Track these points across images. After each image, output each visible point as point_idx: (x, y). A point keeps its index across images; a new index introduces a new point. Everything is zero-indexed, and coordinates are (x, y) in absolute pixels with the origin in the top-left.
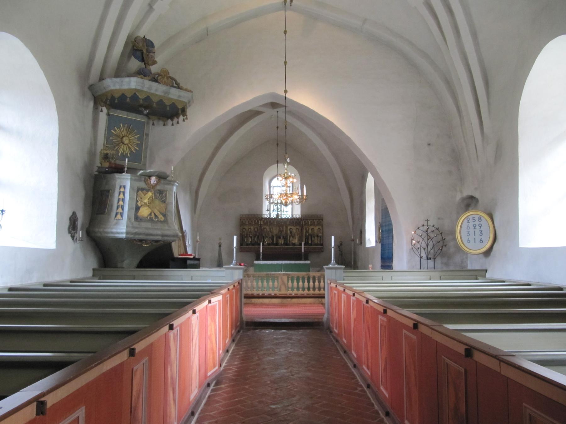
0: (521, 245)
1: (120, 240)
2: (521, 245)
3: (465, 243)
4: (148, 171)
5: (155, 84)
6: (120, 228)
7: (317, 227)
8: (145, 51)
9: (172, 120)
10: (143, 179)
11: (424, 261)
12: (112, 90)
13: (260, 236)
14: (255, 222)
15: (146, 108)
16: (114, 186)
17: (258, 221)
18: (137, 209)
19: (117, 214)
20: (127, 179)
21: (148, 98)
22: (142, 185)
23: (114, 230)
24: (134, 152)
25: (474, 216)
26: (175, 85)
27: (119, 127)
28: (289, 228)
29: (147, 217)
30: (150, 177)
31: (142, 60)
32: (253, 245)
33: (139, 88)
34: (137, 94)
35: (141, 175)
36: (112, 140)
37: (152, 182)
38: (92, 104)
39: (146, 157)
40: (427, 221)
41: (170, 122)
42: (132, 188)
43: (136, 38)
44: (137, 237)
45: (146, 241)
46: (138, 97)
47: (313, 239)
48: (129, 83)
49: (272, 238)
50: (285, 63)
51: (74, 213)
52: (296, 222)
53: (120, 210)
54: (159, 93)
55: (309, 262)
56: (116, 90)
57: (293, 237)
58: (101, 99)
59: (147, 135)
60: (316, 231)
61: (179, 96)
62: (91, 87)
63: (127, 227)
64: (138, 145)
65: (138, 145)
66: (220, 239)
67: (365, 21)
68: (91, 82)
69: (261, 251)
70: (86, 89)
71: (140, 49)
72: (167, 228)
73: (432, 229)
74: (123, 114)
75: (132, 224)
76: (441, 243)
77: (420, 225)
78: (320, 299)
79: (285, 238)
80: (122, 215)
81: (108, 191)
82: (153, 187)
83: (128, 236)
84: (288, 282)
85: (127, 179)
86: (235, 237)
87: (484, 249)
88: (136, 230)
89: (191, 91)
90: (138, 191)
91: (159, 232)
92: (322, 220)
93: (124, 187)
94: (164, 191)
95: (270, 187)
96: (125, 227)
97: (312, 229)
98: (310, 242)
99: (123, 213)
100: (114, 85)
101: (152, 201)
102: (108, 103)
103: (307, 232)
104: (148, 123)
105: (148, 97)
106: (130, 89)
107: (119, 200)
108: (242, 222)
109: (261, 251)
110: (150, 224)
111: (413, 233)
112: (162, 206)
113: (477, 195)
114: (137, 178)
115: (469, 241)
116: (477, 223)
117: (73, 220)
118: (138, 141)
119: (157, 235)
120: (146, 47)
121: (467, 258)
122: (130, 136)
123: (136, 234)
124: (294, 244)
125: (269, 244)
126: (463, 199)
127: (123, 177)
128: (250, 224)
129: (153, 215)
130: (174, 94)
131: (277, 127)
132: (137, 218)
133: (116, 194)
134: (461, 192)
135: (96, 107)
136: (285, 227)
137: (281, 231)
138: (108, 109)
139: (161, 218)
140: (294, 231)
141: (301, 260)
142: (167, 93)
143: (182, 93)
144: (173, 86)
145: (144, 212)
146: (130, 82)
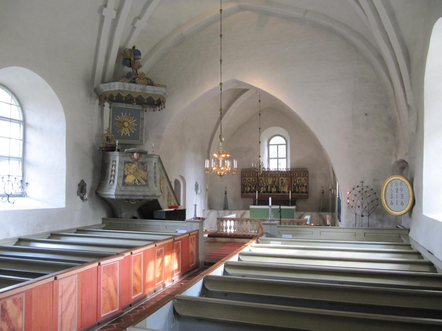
0: (64, 206)
2: (64, 206)
3: (389, 203)
5: (133, 85)
6: (112, 192)
7: (304, 178)
8: (132, 59)
14: (253, 174)
17: (255, 174)
18: (125, 177)
23: (108, 193)
24: (133, 132)
27: (120, 115)
28: (280, 179)
30: (133, 153)
33: (122, 89)
35: (126, 152)
36: (116, 125)
37: (135, 157)
38: (97, 102)
42: (120, 162)
45: (132, 200)
49: (267, 187)
50: (221, 61)
51: (82, 182)
52: (286, 174)
53: (112, 178)
54: (138, 91)
55: (294, 207)
56: (107, 91)
57: (283, 186)
58: (103, 98)
59: (143, 119)
61: (154, 91)
62: (95, 90)
63: (116, 190)
64: (136, 127)
65: (136, 127)
66: (226, 188)
68: (95, 86)
70: (93, 91)
72: (147, 190)
74: (123, 105)
75: (120, 188)
79: (277, 187)
80: (113, 181)
81: (107, 164)
82: (137, 160)
88: (123, 193)
89: (165, 86)
90: (125, 164)
91: (141, 194)
92: (308, 172)
95: (269, 145)
98: (297, 191)
100: (106, 88)
102: (114, 99)
104: (143, 110)
108: (243, 175)
111: (348, 193)
114: (124, 155)
115: (392, 203)
116: (399, 187)
120: (133, 56)
122: (129, 121)
123: (122, 195)
125: (264, 192)
128: (249, 176)
129: (137, 181)
131: (260, 101)
132: (124, 184)
133: (111, 167)
134: (396, 156)
135: (101, 105)
137: (274, 182)
138: (110, 104)
139: (143, 182)
140: (284, 181)
141: (288, 205)
142: (144, 89)
143: (156, 89)
145: (130, 179)
146: (115, 85)
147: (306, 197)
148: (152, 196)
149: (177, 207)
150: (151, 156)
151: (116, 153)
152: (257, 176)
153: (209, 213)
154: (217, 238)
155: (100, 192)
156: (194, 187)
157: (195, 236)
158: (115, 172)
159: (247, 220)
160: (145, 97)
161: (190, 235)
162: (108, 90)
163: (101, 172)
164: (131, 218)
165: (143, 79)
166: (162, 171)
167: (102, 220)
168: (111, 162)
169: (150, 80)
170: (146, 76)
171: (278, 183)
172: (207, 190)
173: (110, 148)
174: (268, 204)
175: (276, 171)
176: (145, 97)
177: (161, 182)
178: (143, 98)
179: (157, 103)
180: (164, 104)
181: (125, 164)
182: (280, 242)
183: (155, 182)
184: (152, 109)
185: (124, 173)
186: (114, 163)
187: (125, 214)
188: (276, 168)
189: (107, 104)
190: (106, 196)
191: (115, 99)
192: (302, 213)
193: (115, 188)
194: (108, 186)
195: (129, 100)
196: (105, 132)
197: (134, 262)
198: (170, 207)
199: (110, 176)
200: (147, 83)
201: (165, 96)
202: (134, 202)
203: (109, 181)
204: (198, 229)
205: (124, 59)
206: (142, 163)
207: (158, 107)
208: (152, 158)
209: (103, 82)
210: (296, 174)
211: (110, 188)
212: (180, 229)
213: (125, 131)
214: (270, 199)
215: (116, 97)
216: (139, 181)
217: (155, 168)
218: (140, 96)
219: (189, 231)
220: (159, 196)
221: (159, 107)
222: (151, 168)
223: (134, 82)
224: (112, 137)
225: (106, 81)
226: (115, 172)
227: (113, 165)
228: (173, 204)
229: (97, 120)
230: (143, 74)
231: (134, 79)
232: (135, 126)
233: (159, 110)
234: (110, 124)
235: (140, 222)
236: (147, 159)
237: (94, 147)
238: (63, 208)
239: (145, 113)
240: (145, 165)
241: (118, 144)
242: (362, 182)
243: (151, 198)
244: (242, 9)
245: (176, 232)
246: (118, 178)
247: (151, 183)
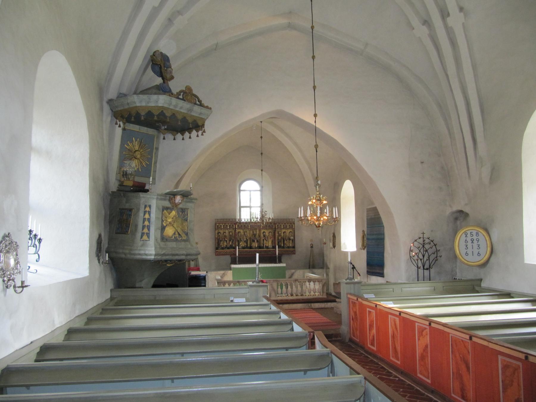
0: (526, 261)
2: (526, 261)
6: (150, 250)
7: (289, 230)
8: (162, 66)
9: (183, 135)
10: (168, 198)
11: (421, 271)
12: (136, 107)
13: (235, 239)
14: (230, 226)
15: (164, 123)
17: (233, 226)
18: (163, 228)
19: (143, 234)
21: (162, 114)
22: (167, 204)
24: (145, 166)
25: (471, 231)
26: (197, 102)
28: (262, 231)
29: (172, 237)
31: (161, 75)
32: (228, 248)
33: (166, 106)
40: (423, 233)
41: (179, 136)
42: (157, 207)
43: (155, 52)
44: (165, 258)
47: (285, 242)
48: (157, 102)
50: (314, 87)
53: (146, 230)
55: (283, 265)
56: (141, 106)
59: (157, 149)
60: (287, 234)
63: (156, 248)
67: (366, 45)
69: (237, 255)
71: (159, 63)
73: (427, 241)
75: (159, 245)
76: (436, 254)
77: (417, 238)
78: (310, 304)
80: (148, 235)
81: (131, 210)
83: (156, 257)
84: (278, 288)
87: (482, 262)
90: (163, 211)
91: (184, 252)
92: (294, 224)
93: (150, 206)
96: (153, 248)
97: (284, 233)
99: (149, 233)
100: (141, 102)
101: (175, 220)
102: (133, 119)
103: (279, 235)
104: (158, 137)
105: (174, 114)
106: (157, 106)
107: (144, 220)
109: (237, 255)
110: (175, 243)
113: (466, 210)
114: (163, 197)
115: (467, 254)
116: (475, 237)
117: (99, 242)
119: (183, 255)
121: (456, 267)
122: (141, 151)
123: (164, 255)
124: (267, 247)
125: (243, 248)
126: (453, 213)
129: (177, 235)
130: (197, 111)
132: (164, 239)
133: (141, 214)
136: (258, 231)
138: (124, 123)
139: (184, 237)
140: (267, 234)
141: (276, 263)
142: (190, 110)
143: (197, 109)
144: (195, 104)
145: (169, 231)
147: (294, 253)
152: (235, 228)
154: (312, 304)
158: (149, 222)
159: (229, 283)
162: (144, 104)
171: (259, 236)
174: (254, 262)
175: (249, 223)
181: (163, 211)
182: (391, 302)
185: (162, 224)
188: (249, 218)
192: (293, 271)
194: (138, 242)
197: (374, 339)
210: (281, 226)
214: (257, 255)
216: (179, 234)
226: (149, 222)
238: (87, 277)
242: (423, 233)
244: (290, 26)
245: (232, 301)
246: (156, 230)
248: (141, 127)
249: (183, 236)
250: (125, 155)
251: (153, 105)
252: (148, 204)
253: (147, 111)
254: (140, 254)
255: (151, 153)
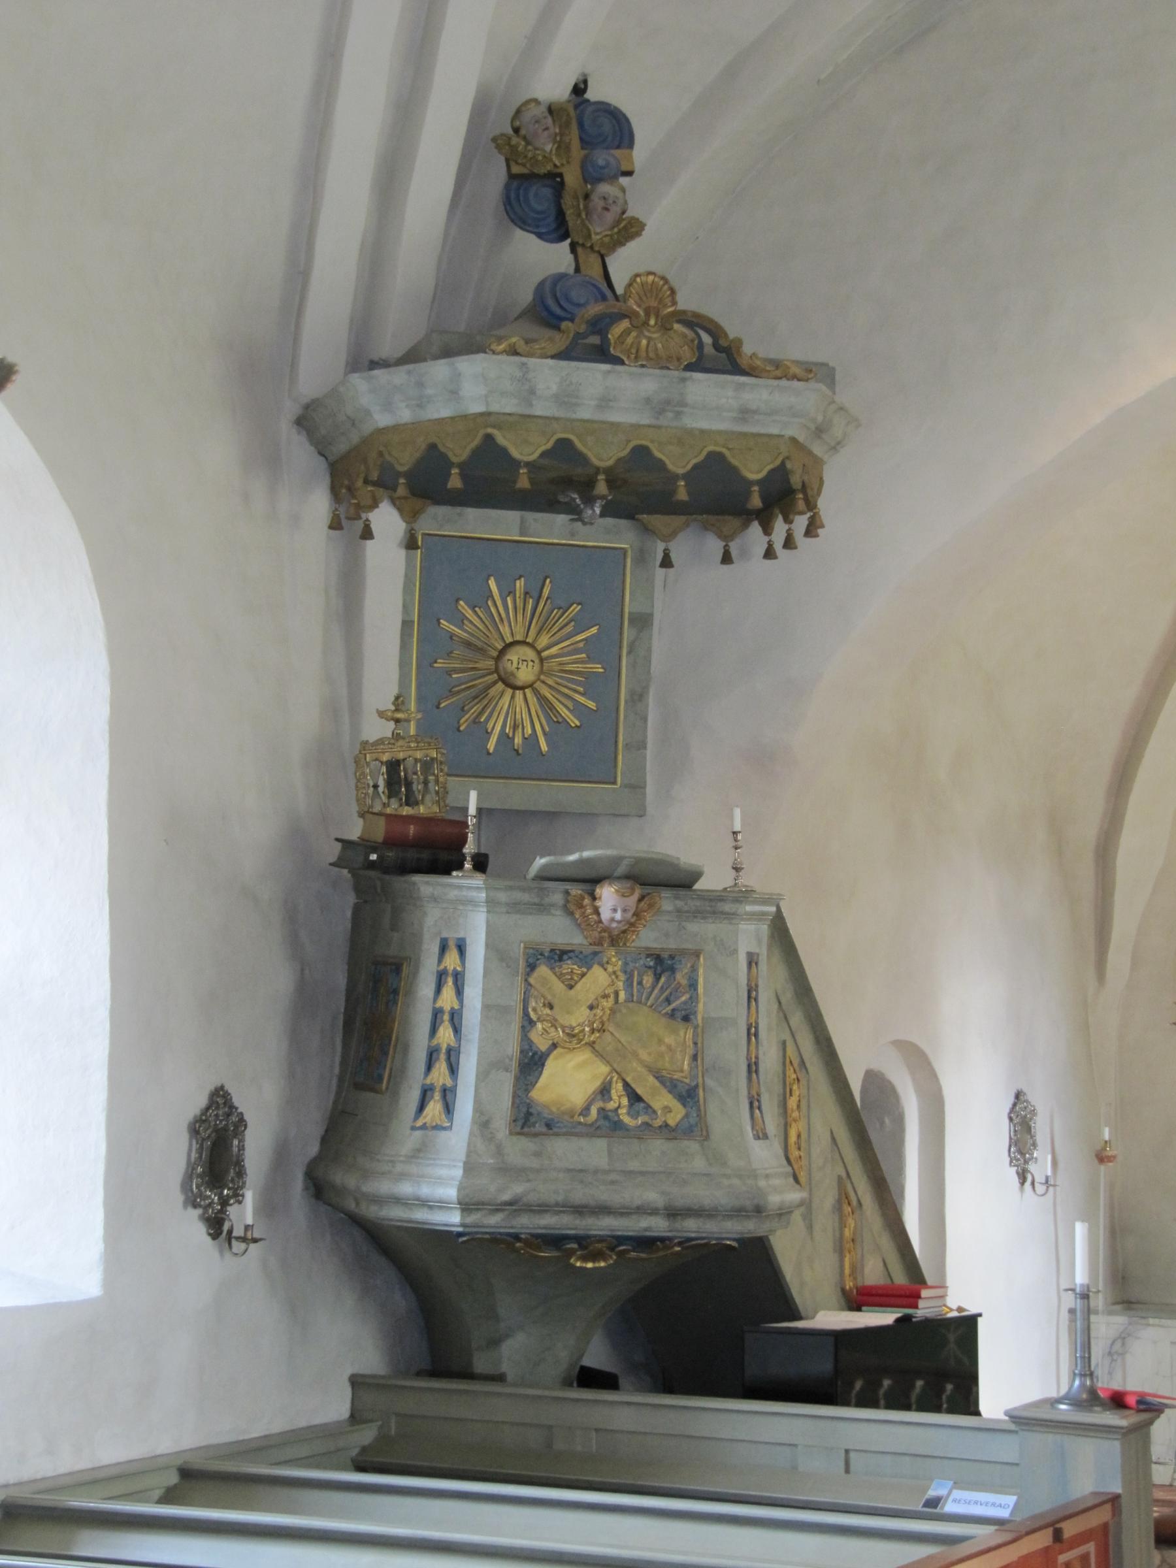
1: (440, 1238)
4: (572, 858)
5: (592, 377)
6: (437, 1177)
8: (572, 178)
10: (558, 898)
12: (381, 431)
16: (417, 939)
18: (531, 1063)
19: (426, 1094)
20: (472, 902)
23: (406, 1189)
29: (586, 1110)
33: (508, 406)
34: (501, 439)
35: (544, 877)
36: (454, 673)
37: (606, 915)
38: (319, 504)
39: (643, 745)
44: (526, 1224)
45: (586, 1244)
46: (504, 452)
51: (220, 1099)
56: (396, 428)
58: (358, 474)
59: (643, 621)
61: (745, 413)
62: (307, 421)
65: (590, 684)
68: (309, 385)
70: (285, 428)
75: (499, 1151)
81: (397, 968)
82: (616, 939)
83: (472, 1218)
85: (472, 902)
86: (1080, 1229)
88: (517, 1189)
91: (652, 1196)
93: (461, 949)
94: (683, 952)
96: (458, 1173)
100: (389, 405)
102: (455, 482)
104: (641, 558)
106: (465, 417)
110: (601, 1144)
112: (669, 1040)
114: (526, 897)
118: (590, 659)
120: (577, 152)
122: (543, 641)
123: (515, 1206)
127: (453, 894)
129: (618, 1098)
132: (528, 1119)
133: (425, 989)
135: (348, 520)
138: (411, 516)
139: (673, 1111)
143: (758, 393)
145: (569, 1081)
146: (456, 376)
148: (739, 1212)
149: (911, 1298)
150: (717, 906)
151: (466, 884)
153: (1123, 1338)
155: (341, 1177)
156: (1004, 1130)
157: (1091, 1547)
160: (678, 462)
161: (1058, 1535)
162: (405, 415)
163: (361, 1024)
164: (567, 1383)
165: (665, 327)
166: (797, 1019)
167: (348, 1392)
168: (431, 948)
169: (715, 331)
170: (681, 306)
172: (1102, 1158)
173: (418, 844)
176: (678, 462)
177: (792, 1102)
178: (661, 466)
179: (760, 499)
180: (811, 505)
181: (532, 967)
183: (754, 1103)
184: (715, 546)
186: (451, 961)
187: (527, 1345)
189: (387, 520)
190: (395, 1213)
191: (446, 477)
193: (461, 1154)
194: (403, 1136)
195: (562, 481)
196: (377, 729)
198: (857, 1300)
199: (419, 1056)
200: (688, 356)
201: (818, 449)
202: (594, 1257)
203: (412, 1096)
204: (1119, 1490)
205: (512, 176)
206: (658, 959)
207: (755, 528)
208: (730, 916)
209: (363, 361)
211: (419, 1152)
212: (957, 1485)
213: (512, 717)
215: (465, 468)
216: (635, 1098)
217: (752, 995)
218: (641, 453)
219: (1045, 1501)
220: (783, 1214)
221: (767, 529)
222: (719, 993)
223: (602, 354)
224: (427, 765)
225: (388, 347)
226: (457, 1030)
227: (441, 977)
228: (873, 1275)
229: (329, 634)
230: (657, 290)
231: (600, 325)
232: (588, 676)
233: (769, 554)
234: (404, 664)
235: (634, 1413)
236: (693, 927)
237: (296, 838)
239: (660, 573)
240: (681, 977)
241: (480, 810)
243: (730, 1230)
245: (934, 1503)
246: (483, 1076)
247: (726, 1110)
248: (531, 516)
249: (657, 1105)
250: (449, 673)
251: (445, 412)
252: (452, 935)
253: (422, 443)
254: (398, 1200)
255: (605, 649)
